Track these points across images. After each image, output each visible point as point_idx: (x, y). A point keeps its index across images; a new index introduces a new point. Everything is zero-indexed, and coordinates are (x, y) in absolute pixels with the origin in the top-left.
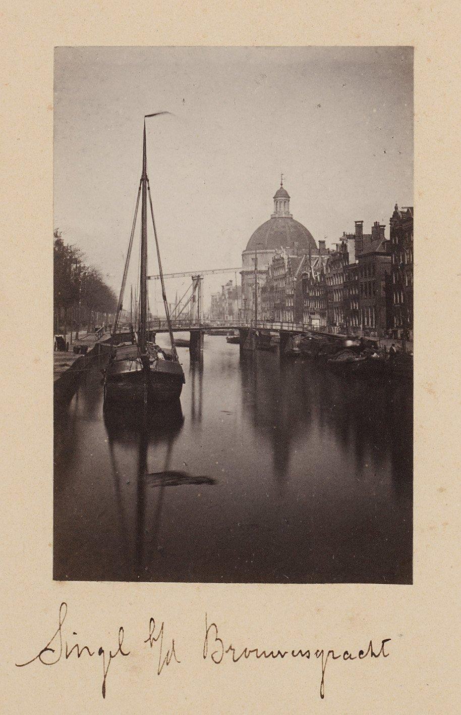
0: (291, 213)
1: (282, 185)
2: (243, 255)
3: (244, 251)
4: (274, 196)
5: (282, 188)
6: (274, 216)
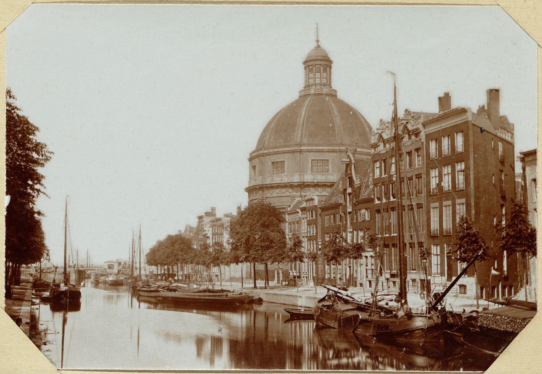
2: (250, 160)
3: (253, 152)
5: (319, 46)
6: (307, 92)
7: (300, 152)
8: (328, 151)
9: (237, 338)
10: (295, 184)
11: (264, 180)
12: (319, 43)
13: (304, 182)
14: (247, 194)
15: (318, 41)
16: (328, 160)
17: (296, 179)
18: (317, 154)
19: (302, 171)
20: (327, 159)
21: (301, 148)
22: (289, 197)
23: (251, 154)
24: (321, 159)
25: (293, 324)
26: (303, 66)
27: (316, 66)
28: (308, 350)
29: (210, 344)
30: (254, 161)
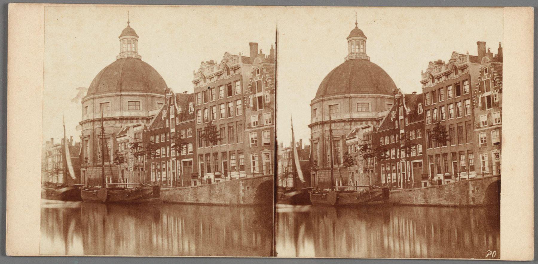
0: (139, 54)
1: (128, 23)
2: (311, 105)
4: (348, 36)
7: (349, 97)
8: (369, 97)
9: (369, 229)
10: (346, 120)
11: (323, 118)
12: (358, 26)
13: (124, 117)
14: (310, 129)
15: (128, 23)
16: (139, 102)
17: (347, 116)
18: (132, 97)
19: (350, 110)
20: (139, 101)
21: (121, 93)
22: (112, 128)
23: (312, 101)
24: (135, 101)
25: (91, 217)
26: (347, 41)
27: (357, 40)
28: (409, 228)
30: (85, 103)
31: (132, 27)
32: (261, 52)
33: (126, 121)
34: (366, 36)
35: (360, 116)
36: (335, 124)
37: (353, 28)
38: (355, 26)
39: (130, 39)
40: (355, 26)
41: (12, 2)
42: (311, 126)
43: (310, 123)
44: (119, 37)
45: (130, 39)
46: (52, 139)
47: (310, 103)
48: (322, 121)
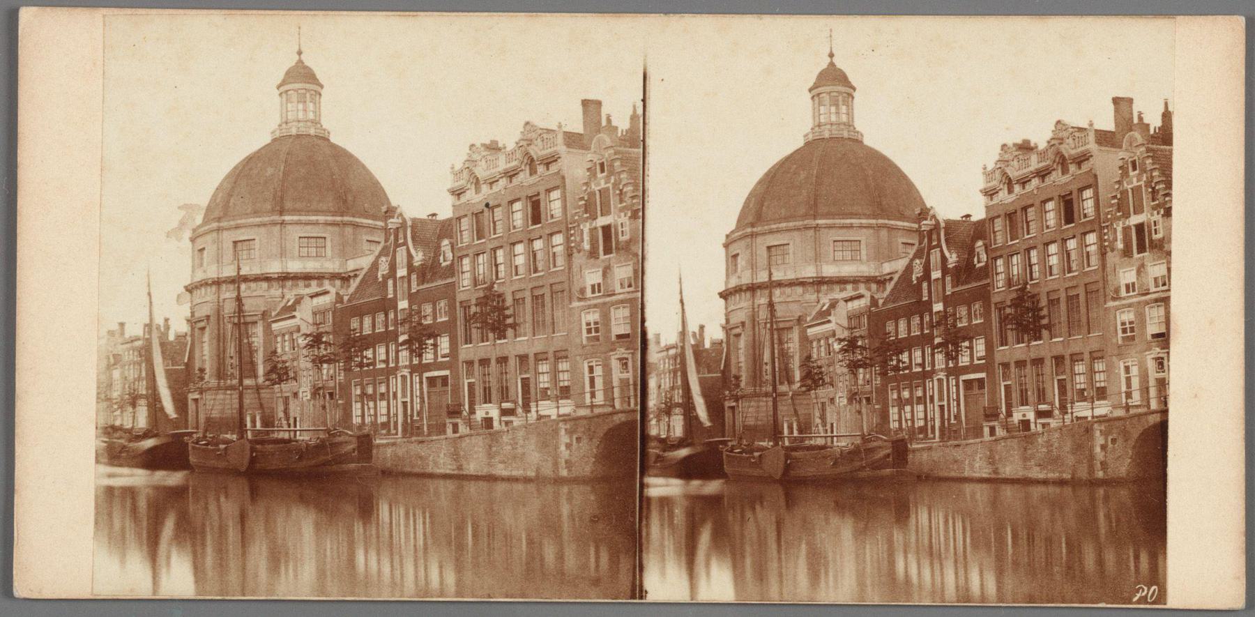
0: (324, 127)
1: (300, 53)
2: (726, 246)
4: (811, 84)
7: (815, 228)
8: (861, 227)
10: (808, 280)
11: (755, 276)
13: (288, 273)
14: (722, 301)
15: (300, 53)
16: (325, 238)
17: (809, 272)
18: (309, 228)
19: (817, 258)
20: (323, 235)
21: (283, 218)
22: (261, 298)
23: (727, 236)
24: (315, 235)
25: (213, 507)
26: (809, 96)
27: (832, 94)
28: (954, 534)
29: (978, 577)
30: (199, 241)
31: (307, 63)
32: (609, 120)
33: (295, 282)
34: (854, 84)
35: (839, 272)
36: (783, 289)
37: (824, 66)
38: (829, 60)
39: (304, 91)
40: (829, 60)
41: (27, 5)
42: (724, 295)
43: (722, 288)
44: (278, 88)
45: (304, 91)
46: (122, 325)
47: (723, 240)
48: (752, 284)
